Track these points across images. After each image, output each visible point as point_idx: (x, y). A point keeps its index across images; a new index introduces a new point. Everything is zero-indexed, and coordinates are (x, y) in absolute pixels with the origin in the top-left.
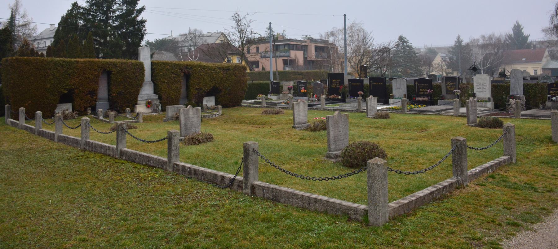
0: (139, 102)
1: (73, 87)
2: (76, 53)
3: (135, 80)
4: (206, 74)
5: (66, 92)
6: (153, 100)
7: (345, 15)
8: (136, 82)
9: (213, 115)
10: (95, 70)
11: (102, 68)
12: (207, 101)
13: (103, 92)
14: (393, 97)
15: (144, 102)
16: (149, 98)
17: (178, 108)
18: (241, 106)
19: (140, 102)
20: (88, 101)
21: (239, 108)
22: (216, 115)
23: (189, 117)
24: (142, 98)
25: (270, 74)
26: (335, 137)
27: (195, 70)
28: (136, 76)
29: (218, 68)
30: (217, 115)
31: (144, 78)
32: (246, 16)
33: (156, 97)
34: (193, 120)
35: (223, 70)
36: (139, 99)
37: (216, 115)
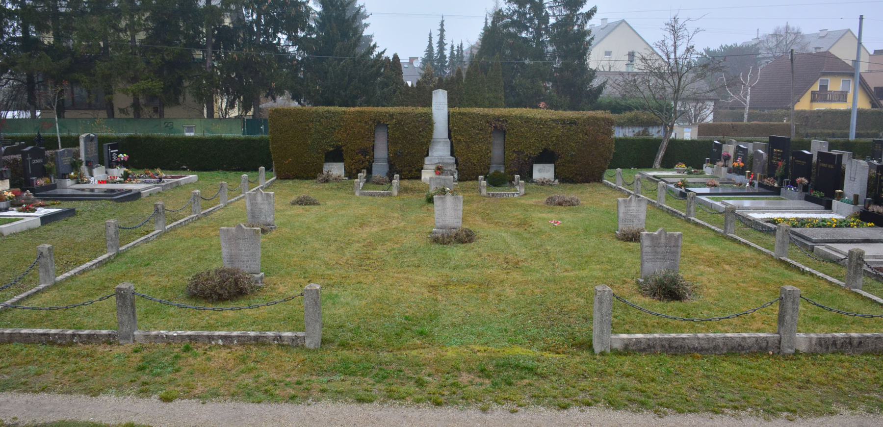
0: (425, 166)
1: (340, 143)
2: (475, 85)
3: (417, 137)
4: (531, 130)
5: (331, 149)
6: (447, 164)
7: (861, 18)
8: (420, 140)
9: (508, 194)
10: (366, 122)
11: (375, 120)
12: (540, 171)
13: (381, 151)
14: (840, 197)
15: (434, 167)
16: (441, 161)
17: (445, 179)
18: (602, 183)
19: (428, 166)
20: (359, 161)
21: (598, 184)
22: (514, 194)
23: (257, 203)
24: (430, 160)
25: (852, 115)
26: (231, 256)
27: (511, 123)
28: (420, 132)
29: (554, 121)
30: (516, 195)
31: (431, 135)
32: (686, 23)
33: (452, 160)
34: (262, 207)
35: (564, 123)
36: (426, 162)
37: (514, 194)
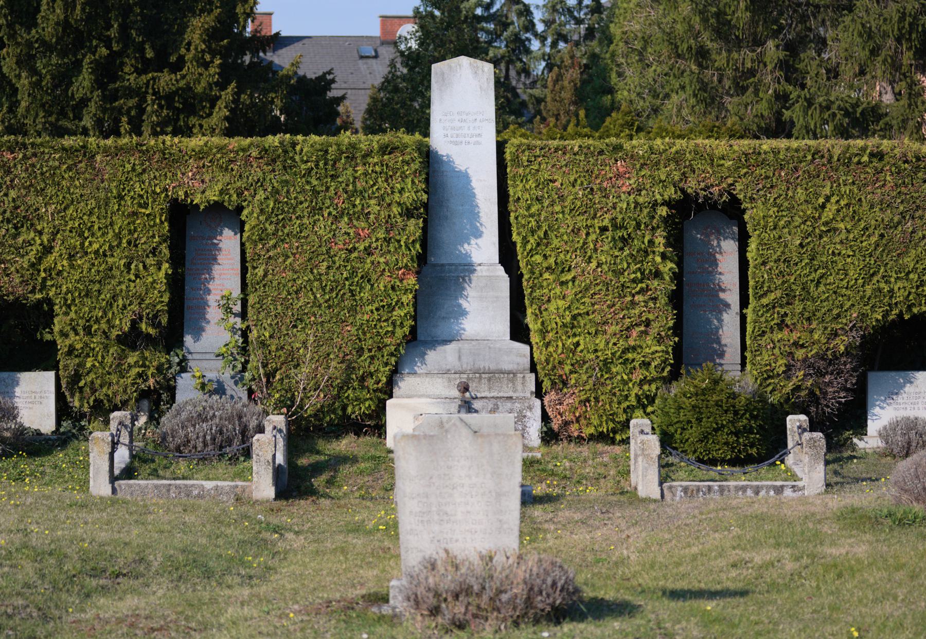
22: (779, 490)
